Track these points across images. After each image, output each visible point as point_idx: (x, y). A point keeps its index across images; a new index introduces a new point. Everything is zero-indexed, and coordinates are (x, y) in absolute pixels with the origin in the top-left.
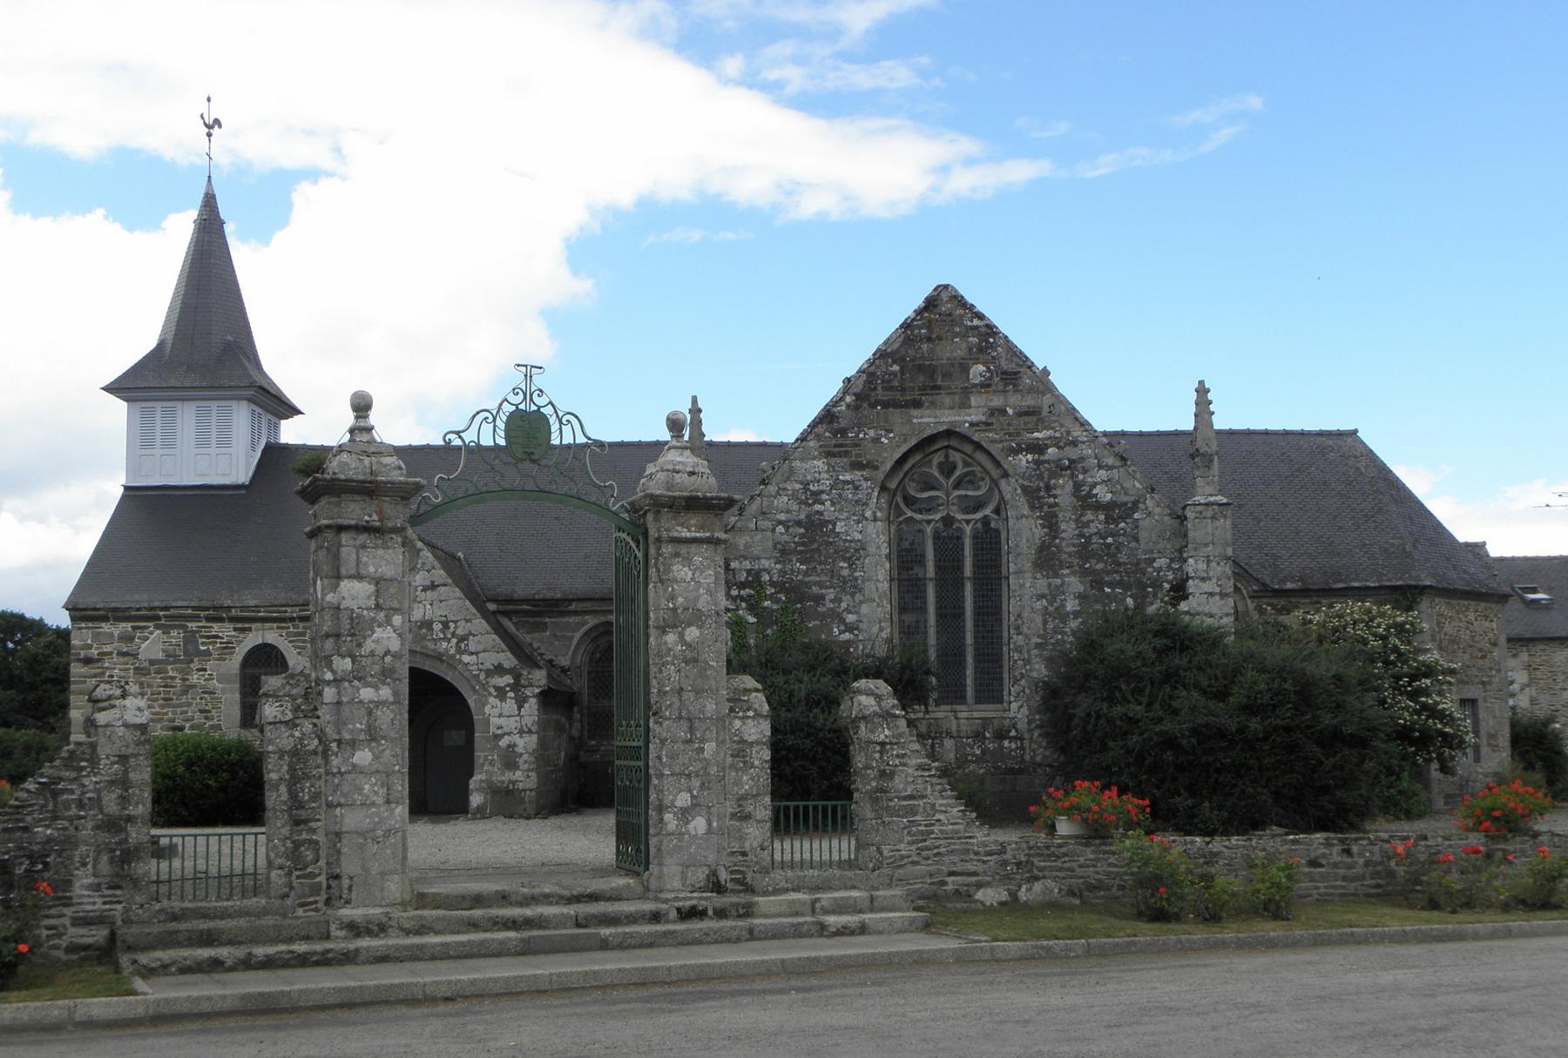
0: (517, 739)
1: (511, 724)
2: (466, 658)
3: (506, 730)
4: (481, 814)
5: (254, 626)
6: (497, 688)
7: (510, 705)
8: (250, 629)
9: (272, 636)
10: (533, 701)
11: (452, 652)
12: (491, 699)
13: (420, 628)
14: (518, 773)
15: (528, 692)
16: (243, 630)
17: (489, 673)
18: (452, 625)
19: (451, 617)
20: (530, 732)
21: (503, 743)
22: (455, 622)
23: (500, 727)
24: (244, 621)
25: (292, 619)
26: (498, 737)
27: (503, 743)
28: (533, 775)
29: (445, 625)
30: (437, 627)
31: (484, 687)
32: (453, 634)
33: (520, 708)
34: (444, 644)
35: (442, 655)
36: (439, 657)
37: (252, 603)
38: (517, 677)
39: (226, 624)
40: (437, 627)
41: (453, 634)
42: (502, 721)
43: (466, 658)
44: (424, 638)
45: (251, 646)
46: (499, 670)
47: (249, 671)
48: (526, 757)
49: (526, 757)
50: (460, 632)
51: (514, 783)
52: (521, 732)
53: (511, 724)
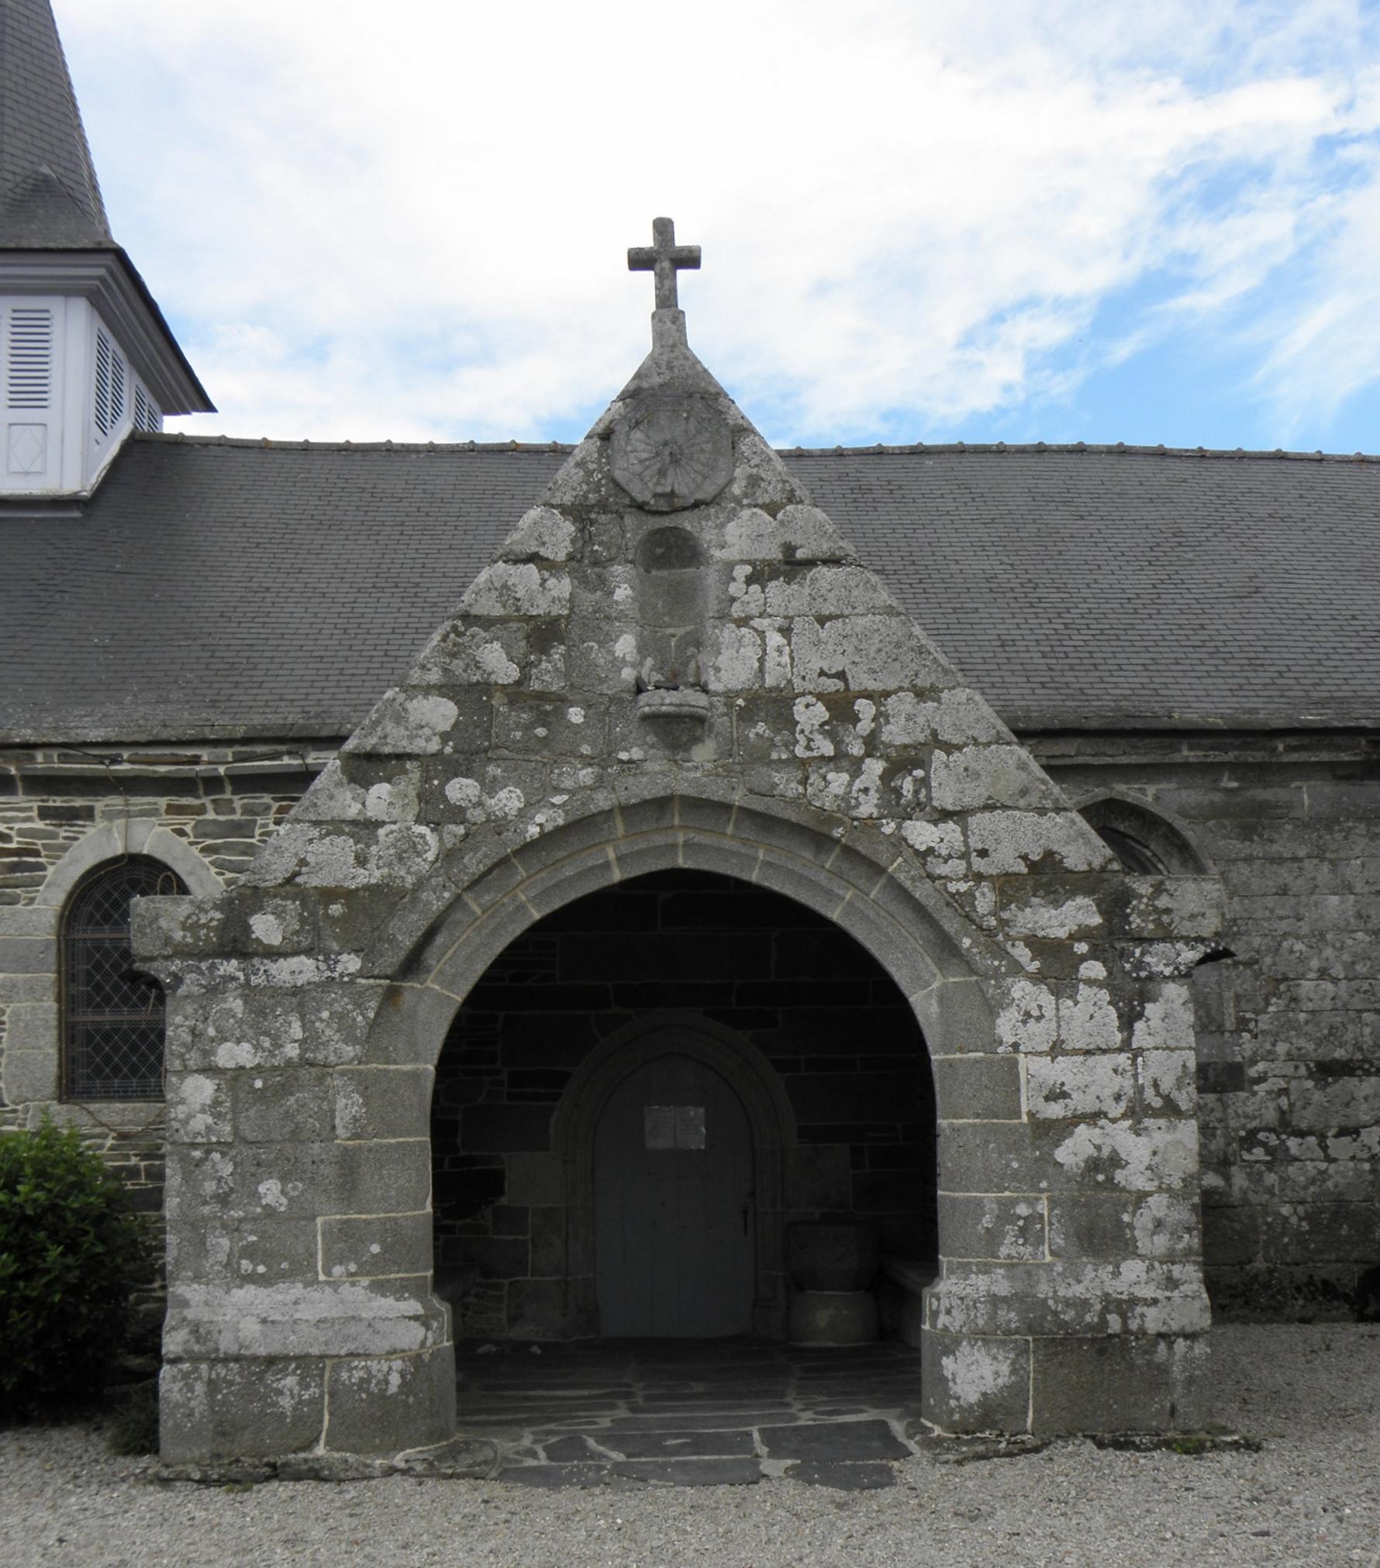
0: (1121, 1138)
1: (1098, 1081)
2: (922, 833)
3: (1081, 1102)
4: (989, 1431)
5: (100, 804)
6: (1039, 946)
7: (1090, 1011)
8: (88, 814)
9: (151, 832)
10: (1175, 993)
11: (868, 807)
12: (1021, 989)
13: (747, 716)
14: (1133, 1269)
15: (1157, 959)
16: (70, 816)
17: (1009, 888)
18: (864, 708)
19: (861, 680)
20: (1171, 1109)
21: (1072, 1152)
22: (878, 697)
23: (1057, 1094)
24: (72, 785)
25: (213, 784)
26: (1051, 1131)
27: (1072, 1152)
28: (1191, 1275)
29: (841, 709)
30: (810, 715)
31: (992, 939)
32: (872, 743)
33: (1129, 1020)
34: (838, 781)
35: (830, 819)
36: (815, 833)
37: (95, 734)
38: (1115, 905)
39: (20, 799)
40: (810, 715)
41: (872, 743)
42: (1061, 1071)
43: (922, 833)
44: (760, 756)
45: (90, 861)
46: (1047, 876)
47: (86, 934)
48: (1158, 1205)
49: (1158, 1205)
50: (895, 734)
51: (1125, 1306)
52: (1137, 1112)
53: (1098, 1081)
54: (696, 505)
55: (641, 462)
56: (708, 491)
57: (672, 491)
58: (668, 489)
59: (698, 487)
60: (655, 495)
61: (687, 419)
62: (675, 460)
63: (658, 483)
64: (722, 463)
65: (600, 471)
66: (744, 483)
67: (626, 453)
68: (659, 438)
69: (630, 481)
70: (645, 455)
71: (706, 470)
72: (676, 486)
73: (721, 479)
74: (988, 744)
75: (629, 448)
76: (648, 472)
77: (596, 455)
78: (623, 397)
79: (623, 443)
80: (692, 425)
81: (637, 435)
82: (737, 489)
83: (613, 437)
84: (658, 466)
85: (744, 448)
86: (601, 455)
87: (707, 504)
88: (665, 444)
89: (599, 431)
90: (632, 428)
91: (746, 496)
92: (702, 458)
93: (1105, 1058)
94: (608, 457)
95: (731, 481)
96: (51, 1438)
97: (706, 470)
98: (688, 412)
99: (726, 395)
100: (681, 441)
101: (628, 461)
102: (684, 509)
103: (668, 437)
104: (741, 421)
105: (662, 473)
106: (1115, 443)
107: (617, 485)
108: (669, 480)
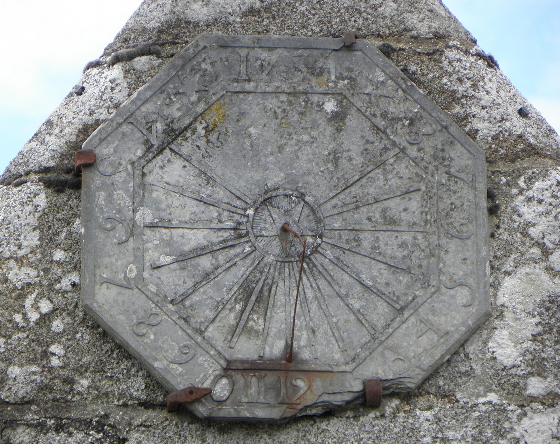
54: (369, 399)
55: (184, 258)
56: (409, 353)
57: (290, 355)
58: (275, 348)
59: (377, 339)
60: (230, 368)
61: (338, 118)
62: (300, 256)
63: (239, 329)
64: (455, 259)
65: (49, 290)
66: (530, 326)
67: (133, 231)
68: (245, 180)
69: (146, 322)
70: (196, 238)
71: (400, 284)
72: (302, 339)
73: (453, 312)
74: (212, 142)
75: (145, 215)
76: (207, 292)
77: (32, 239)
78: (122, 53)
79: (123, 199)
80: (355, 139)
81: (171, 171)
82: (505, 347)
83: (92, 180)
84: (242, 270)
85: (528, 212)
86: (49, 240)
87: (408, 396)
88: (267, 200)
89: (45, 157)
90: (153, 151)
91: (538, 367)
92: (390, 244)
93: (376, 352)
94: (74, 245)
95: (485, 322)
96: (267, 99)
97: (400, 284)
98: (340, 97)
99: (468, 42)
100: (319, 189)
101: (139, 260)
102: (330, 412)
103: (275, 178)
104: (517, 125)
105: (254, 296)
106: (15, 155)
107: (103, 333)
108: (279, 318)
